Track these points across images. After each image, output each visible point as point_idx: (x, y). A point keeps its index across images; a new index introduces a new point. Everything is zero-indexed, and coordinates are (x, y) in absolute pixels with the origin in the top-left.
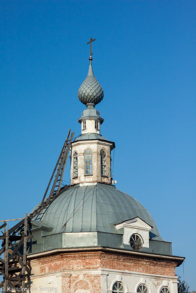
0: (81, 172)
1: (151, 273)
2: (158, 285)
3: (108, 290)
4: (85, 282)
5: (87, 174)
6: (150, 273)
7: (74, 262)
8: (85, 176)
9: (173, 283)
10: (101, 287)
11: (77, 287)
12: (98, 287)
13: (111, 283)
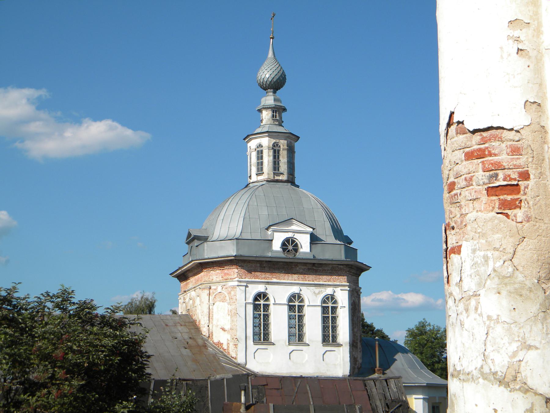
0: (254, 170)
1: (310, 281)
2: (319, 293)
3: (246, 302)
4: (223, 294)
5: (260, 171)
6: (309, 281)
7: (213, 272)
8: (257, 174)
9: (341, 290)
10: (237, 299)
11: (216, 300)
12: (235, 298)
13: (251, 295)
